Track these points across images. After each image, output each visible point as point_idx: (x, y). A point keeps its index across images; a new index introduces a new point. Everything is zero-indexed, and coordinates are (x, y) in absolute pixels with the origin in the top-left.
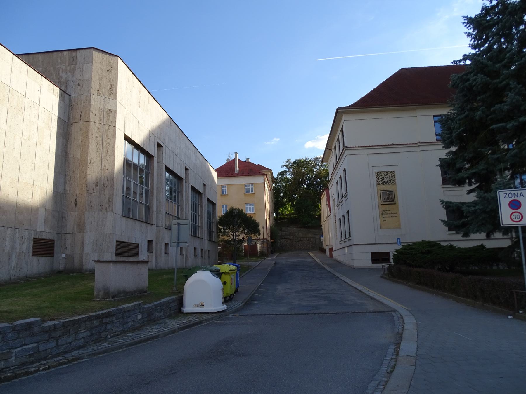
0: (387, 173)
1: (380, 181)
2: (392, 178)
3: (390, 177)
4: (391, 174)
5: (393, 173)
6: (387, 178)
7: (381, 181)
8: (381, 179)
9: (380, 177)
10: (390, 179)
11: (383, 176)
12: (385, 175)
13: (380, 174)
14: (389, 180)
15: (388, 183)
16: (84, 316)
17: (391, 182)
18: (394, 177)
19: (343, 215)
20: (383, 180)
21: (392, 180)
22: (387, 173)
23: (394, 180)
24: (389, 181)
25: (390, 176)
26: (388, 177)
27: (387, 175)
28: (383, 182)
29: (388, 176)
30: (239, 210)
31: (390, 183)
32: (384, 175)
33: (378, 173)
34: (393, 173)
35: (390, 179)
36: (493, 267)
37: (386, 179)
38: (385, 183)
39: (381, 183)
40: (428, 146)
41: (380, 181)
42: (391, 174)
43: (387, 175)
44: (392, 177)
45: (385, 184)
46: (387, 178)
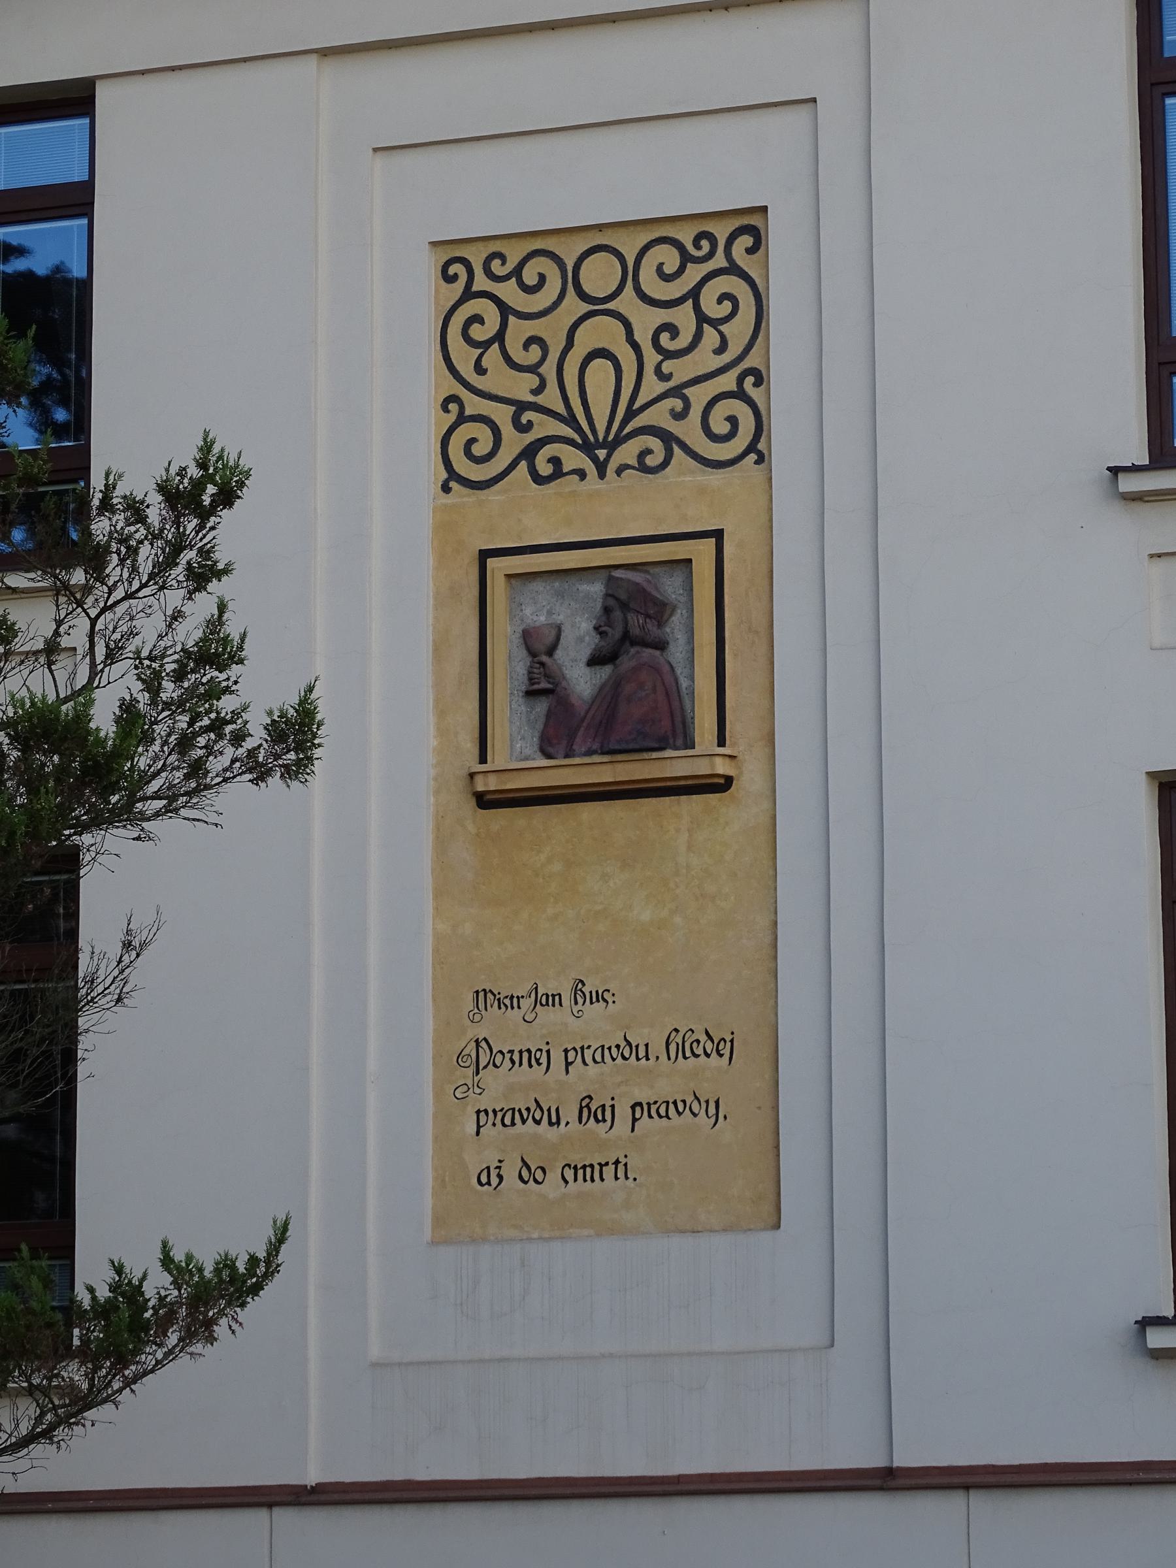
0: (630, 274)
1: (502, 415)
2: (704, 359)
3: (672, 329)
4: (694, 273)
5: (733, 269)
6: (627, 357)
7: (522, 407)
8: (521, 387)
9: (500, 337)
10: (683, 371)
11: (553, 330)
12: (598, 306)
13: (508, 291)
14: (652, 386)
15: (627, 453)
16: (433, 325)
17: (690, 430)
18: (739, 330)
19: (646, 1043)
20: (551, 398)
21: (699, 396)
22: (630, 274)
23: (740, 394)
24: (658, 416)
25: (684, 318)
26: (643, 337)
27: (627, 303)
28: (545, 426)
29: (645, 320)
30: (437, 792)
31: (667, 438)
32: (573, 307)
33: (481, 282)
34: (733, 269)
35: (683, 371)
36: (597, 1154)
37: (601, 370)
38: (587, 447)
39: (514, 443)
40: (667, 121)
41: (502, 415)
42: (694, 273)
43: (627, 303)
44: (711, 337)
45: (573, 458)
46: (627, 357)
